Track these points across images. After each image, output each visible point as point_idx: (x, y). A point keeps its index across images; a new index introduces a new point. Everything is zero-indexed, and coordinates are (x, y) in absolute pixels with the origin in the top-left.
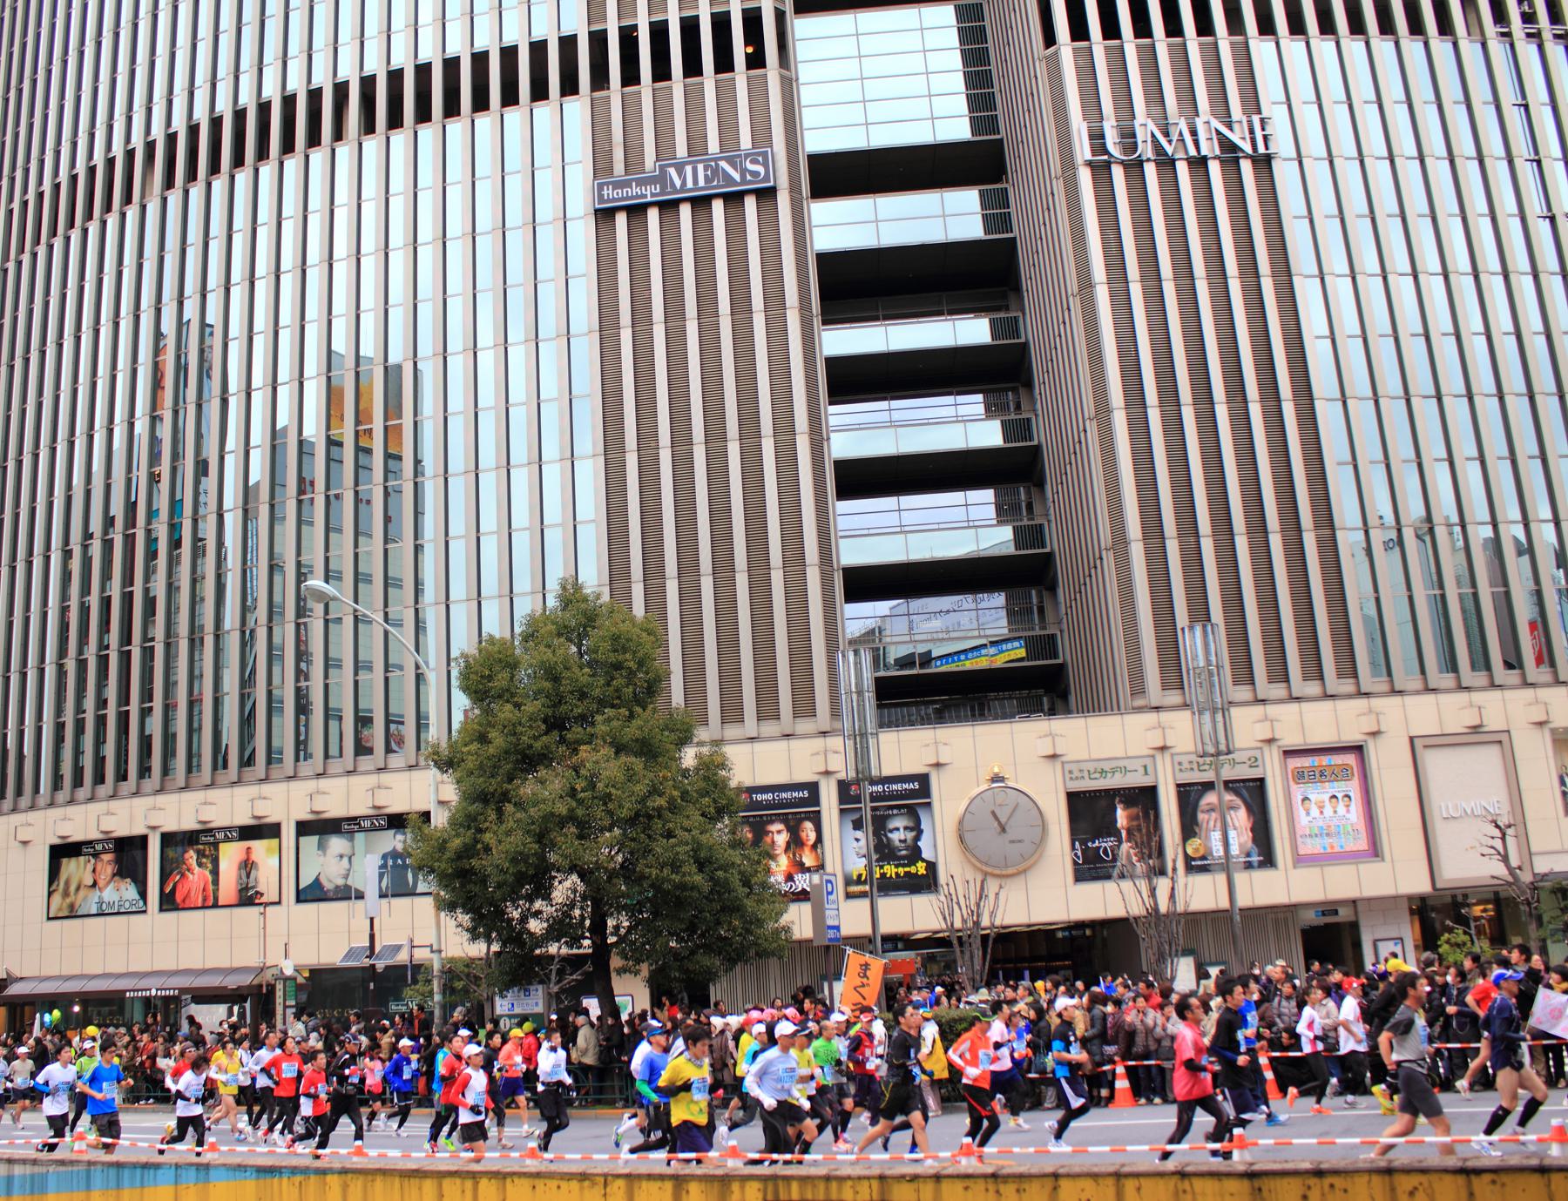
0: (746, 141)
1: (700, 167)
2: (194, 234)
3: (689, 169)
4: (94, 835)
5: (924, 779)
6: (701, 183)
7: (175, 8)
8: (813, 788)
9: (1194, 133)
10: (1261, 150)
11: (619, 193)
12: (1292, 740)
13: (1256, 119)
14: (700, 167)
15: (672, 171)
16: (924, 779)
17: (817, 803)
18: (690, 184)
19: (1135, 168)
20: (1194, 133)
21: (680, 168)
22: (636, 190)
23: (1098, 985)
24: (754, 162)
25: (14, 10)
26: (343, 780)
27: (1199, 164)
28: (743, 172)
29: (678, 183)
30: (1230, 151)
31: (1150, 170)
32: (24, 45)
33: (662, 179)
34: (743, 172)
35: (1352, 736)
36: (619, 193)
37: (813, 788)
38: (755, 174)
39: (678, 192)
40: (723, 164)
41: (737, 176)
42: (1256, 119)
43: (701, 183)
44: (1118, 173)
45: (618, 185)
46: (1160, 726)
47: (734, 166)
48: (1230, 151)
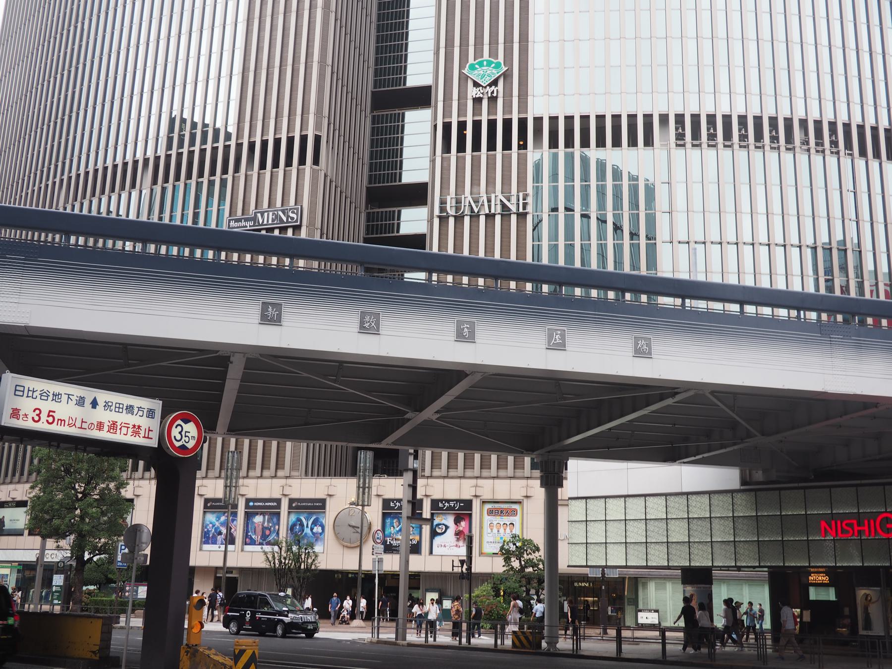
0: (292, 202)
1: (271, 214)
2: (179, 81)
3: (266, 214)
4: (9, 499)
5: (323, 501)
6: (270, 222)
7: (134, 4)
8: (278, 501)
9: (489, 201)
10: (521, 210)
11: (237, 224)
12: (487, 496)
13: (521, 195)
14: (271, 214)
15: (259, 215)
16: (323, 501)
17: (383, 513)
18: (265, 222)
19: (459, 219)
20: (489, 201)
21: (262, 214)
22: (243, 223)
23: (528, 629)
24: (293, 212)
25: (50, 4)
26: (255, 481)
27: (490, 217)
28: (288, 217)
29: (261, 222)
30: (506, 212)
31: (467, 220)
32: (59, 17)
33: (254, 219)
34: (288, 217)
35: (516, 497)
36: (237, 224)
37: (278, 501)
38: (292, 218)
39: (259, 225)
40: (280, 213)
41: (285, 219)
42: (521, 195)
43: (270, 222)
44: (451, 221)
45: (237, 221)
46: (476, 486)
47: (284, 213)
48: (506, 212)
